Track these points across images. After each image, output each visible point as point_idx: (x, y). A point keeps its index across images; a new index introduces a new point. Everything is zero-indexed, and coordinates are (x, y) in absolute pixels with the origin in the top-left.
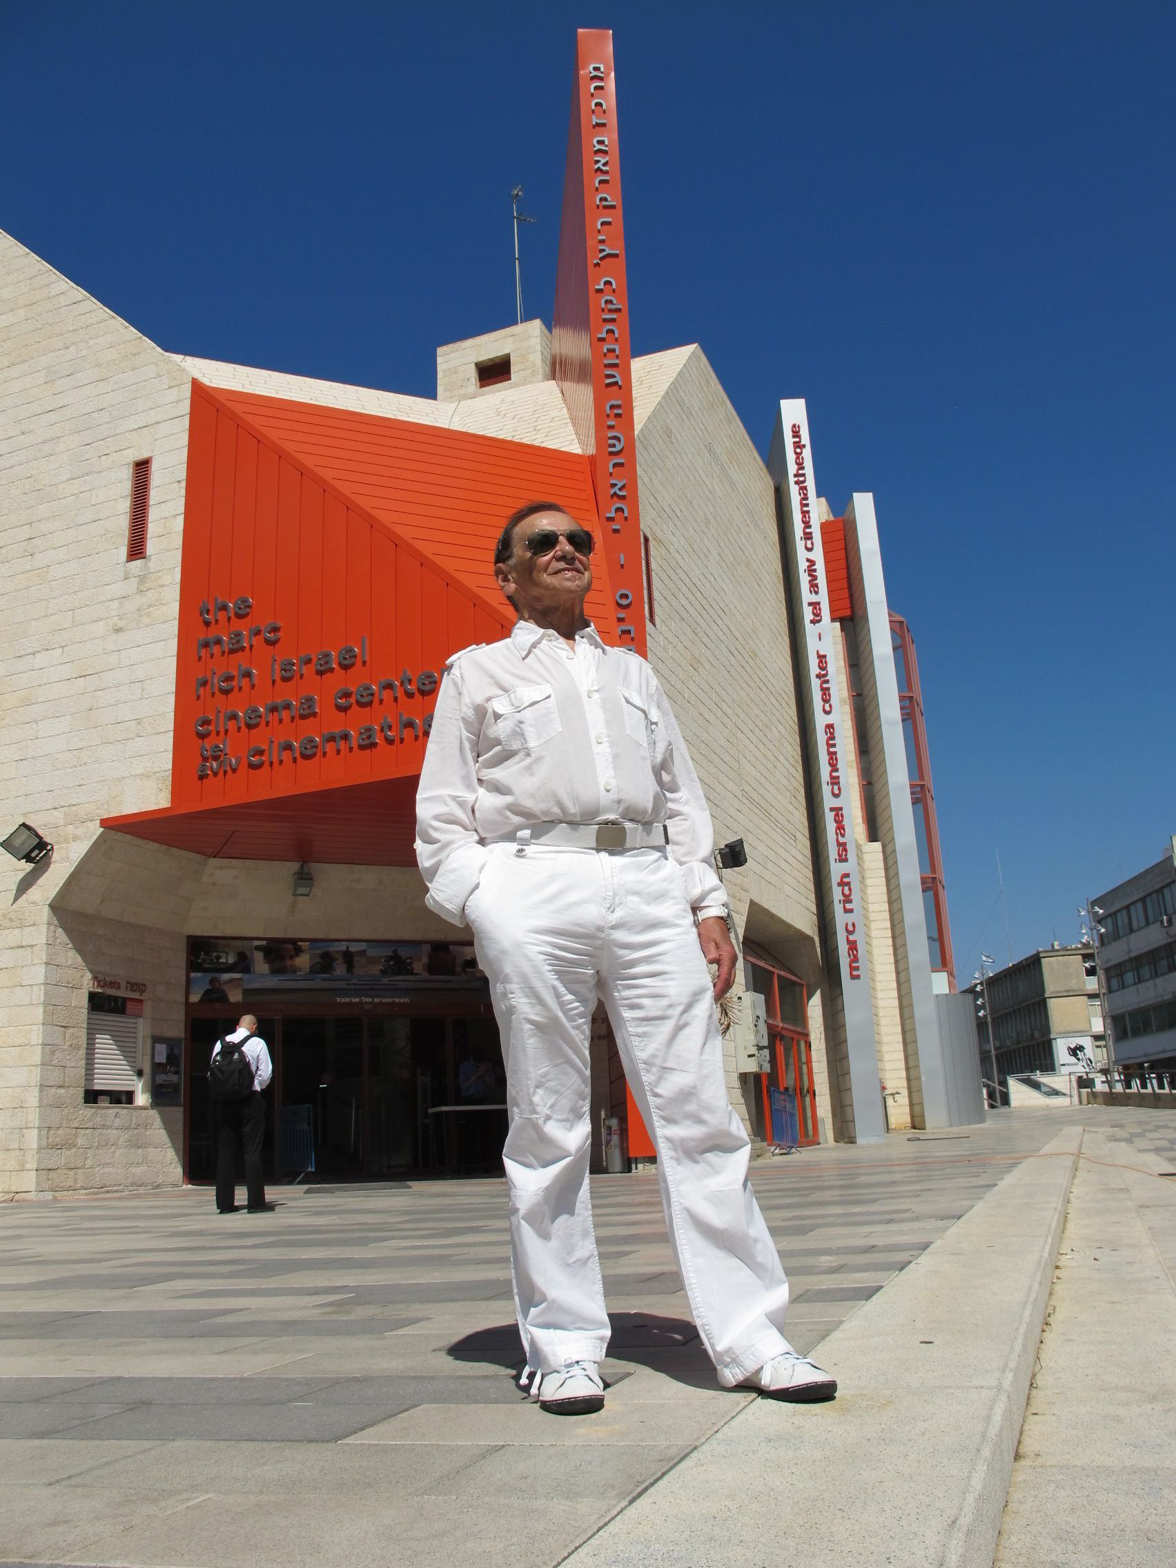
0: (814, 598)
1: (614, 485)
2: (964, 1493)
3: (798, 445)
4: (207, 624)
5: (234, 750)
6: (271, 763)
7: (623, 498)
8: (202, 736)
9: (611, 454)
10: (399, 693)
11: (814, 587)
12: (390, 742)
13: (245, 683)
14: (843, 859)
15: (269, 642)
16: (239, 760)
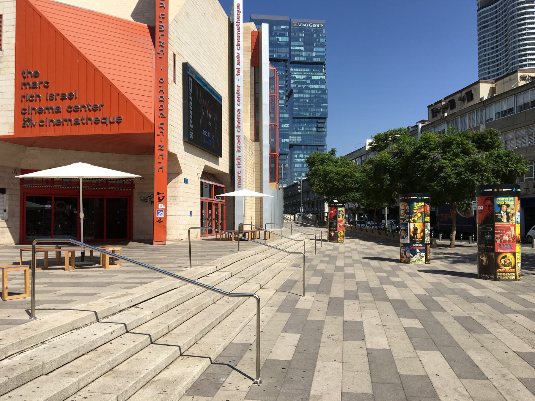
0: (238, 67)
1: (160, 42)
2: (497, 321)
3: (238, 11)
4: (24, 78)
5: (36, 119)
6: (46, 126)
7: (163, 47)
8: (24, 114)
9: (160, 31)
10: (87, 109)
12: (83, 124)
13: (38, 99)
14: (239, 152)
15: (45, 87)
16: (36, 123)
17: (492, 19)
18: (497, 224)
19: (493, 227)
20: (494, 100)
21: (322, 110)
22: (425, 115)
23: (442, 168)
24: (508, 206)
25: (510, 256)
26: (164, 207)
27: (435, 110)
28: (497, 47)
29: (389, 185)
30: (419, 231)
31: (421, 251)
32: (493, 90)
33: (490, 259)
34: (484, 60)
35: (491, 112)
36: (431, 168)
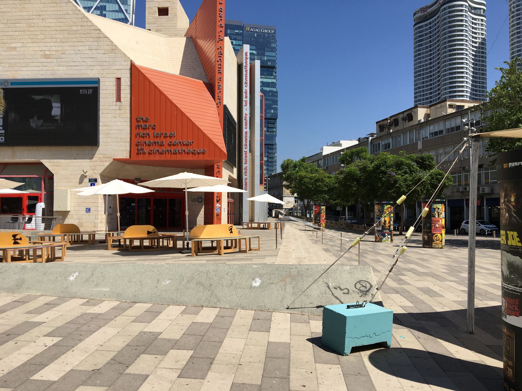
0: (246, 99)
5: (146, 150)
11: (246, 97)
17: (426, 34)
18: (433, 219)
19: (431, 220)
20: (429, 123)
21: (272, 111)
22: (374, 129)
23: (396, 181)
24: (439, 209)
25: (439, 235)
26: (220, 206)
27: (382, 126)
28: (431, 59)
29: (356, 190)
30: (387, 223)
31: (388, 234)
32: (427, 116)
33: (429, 237)
34: (419, 71)
35: (426, 132)
36: (388, 181)
